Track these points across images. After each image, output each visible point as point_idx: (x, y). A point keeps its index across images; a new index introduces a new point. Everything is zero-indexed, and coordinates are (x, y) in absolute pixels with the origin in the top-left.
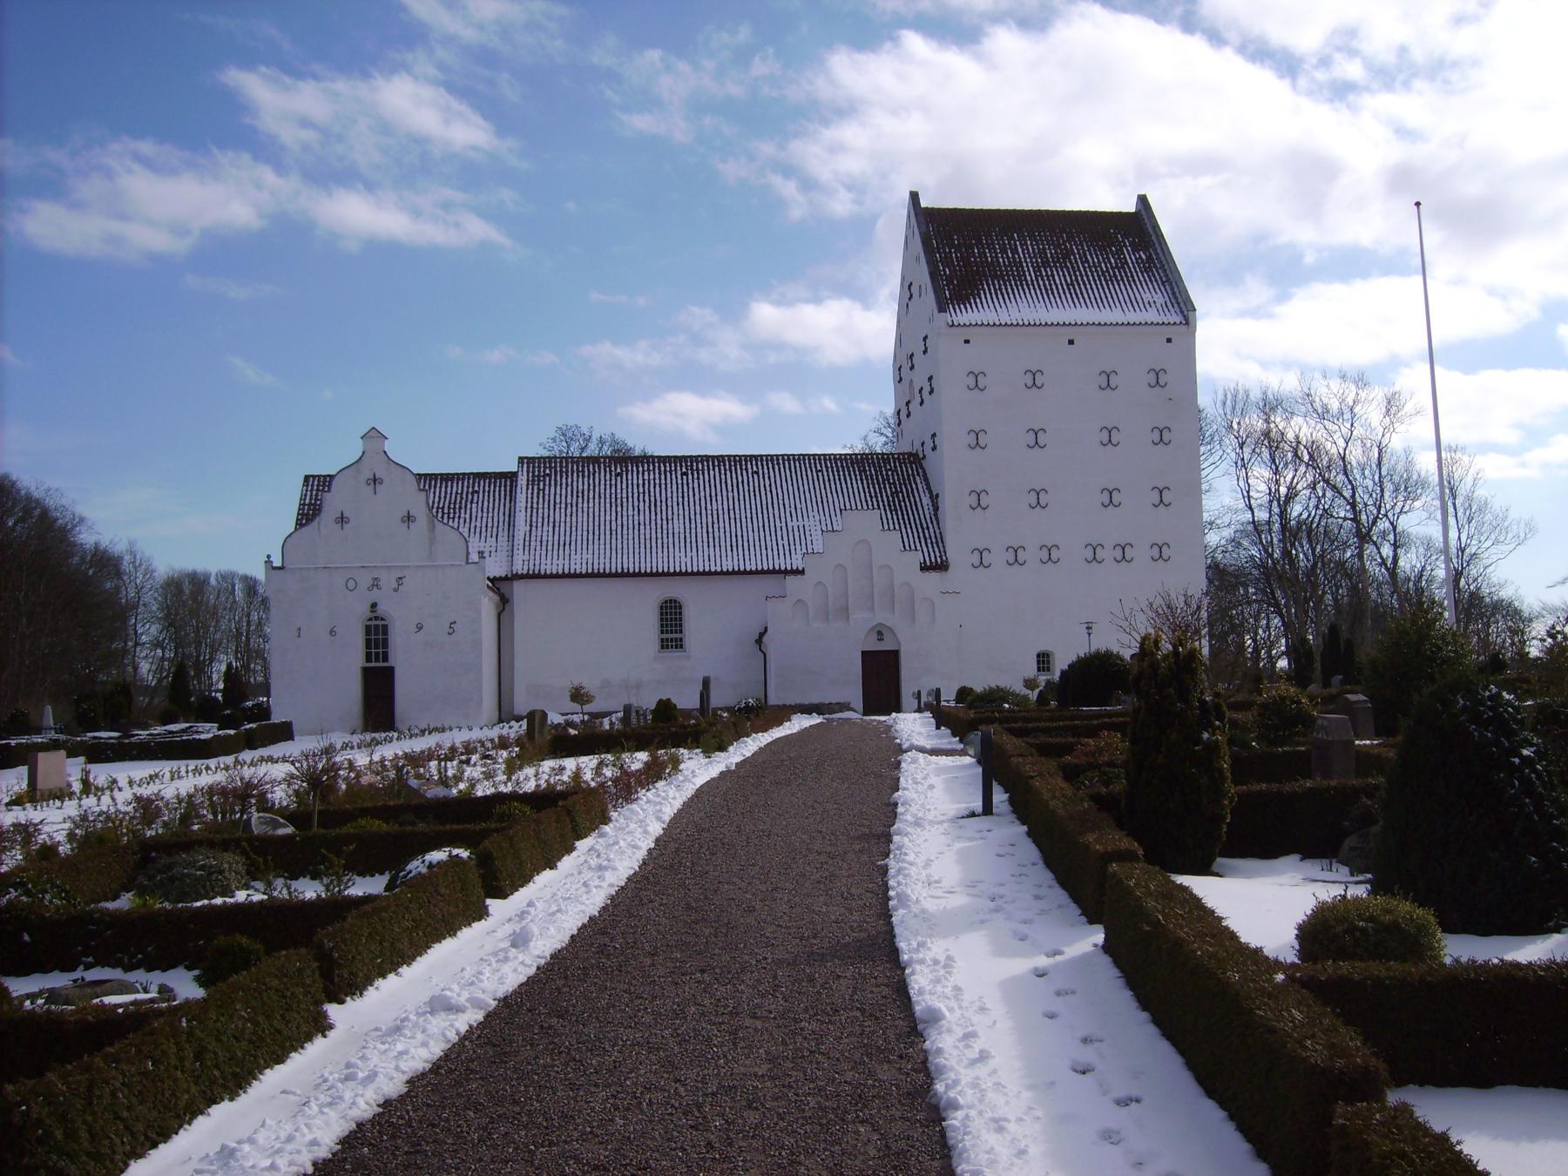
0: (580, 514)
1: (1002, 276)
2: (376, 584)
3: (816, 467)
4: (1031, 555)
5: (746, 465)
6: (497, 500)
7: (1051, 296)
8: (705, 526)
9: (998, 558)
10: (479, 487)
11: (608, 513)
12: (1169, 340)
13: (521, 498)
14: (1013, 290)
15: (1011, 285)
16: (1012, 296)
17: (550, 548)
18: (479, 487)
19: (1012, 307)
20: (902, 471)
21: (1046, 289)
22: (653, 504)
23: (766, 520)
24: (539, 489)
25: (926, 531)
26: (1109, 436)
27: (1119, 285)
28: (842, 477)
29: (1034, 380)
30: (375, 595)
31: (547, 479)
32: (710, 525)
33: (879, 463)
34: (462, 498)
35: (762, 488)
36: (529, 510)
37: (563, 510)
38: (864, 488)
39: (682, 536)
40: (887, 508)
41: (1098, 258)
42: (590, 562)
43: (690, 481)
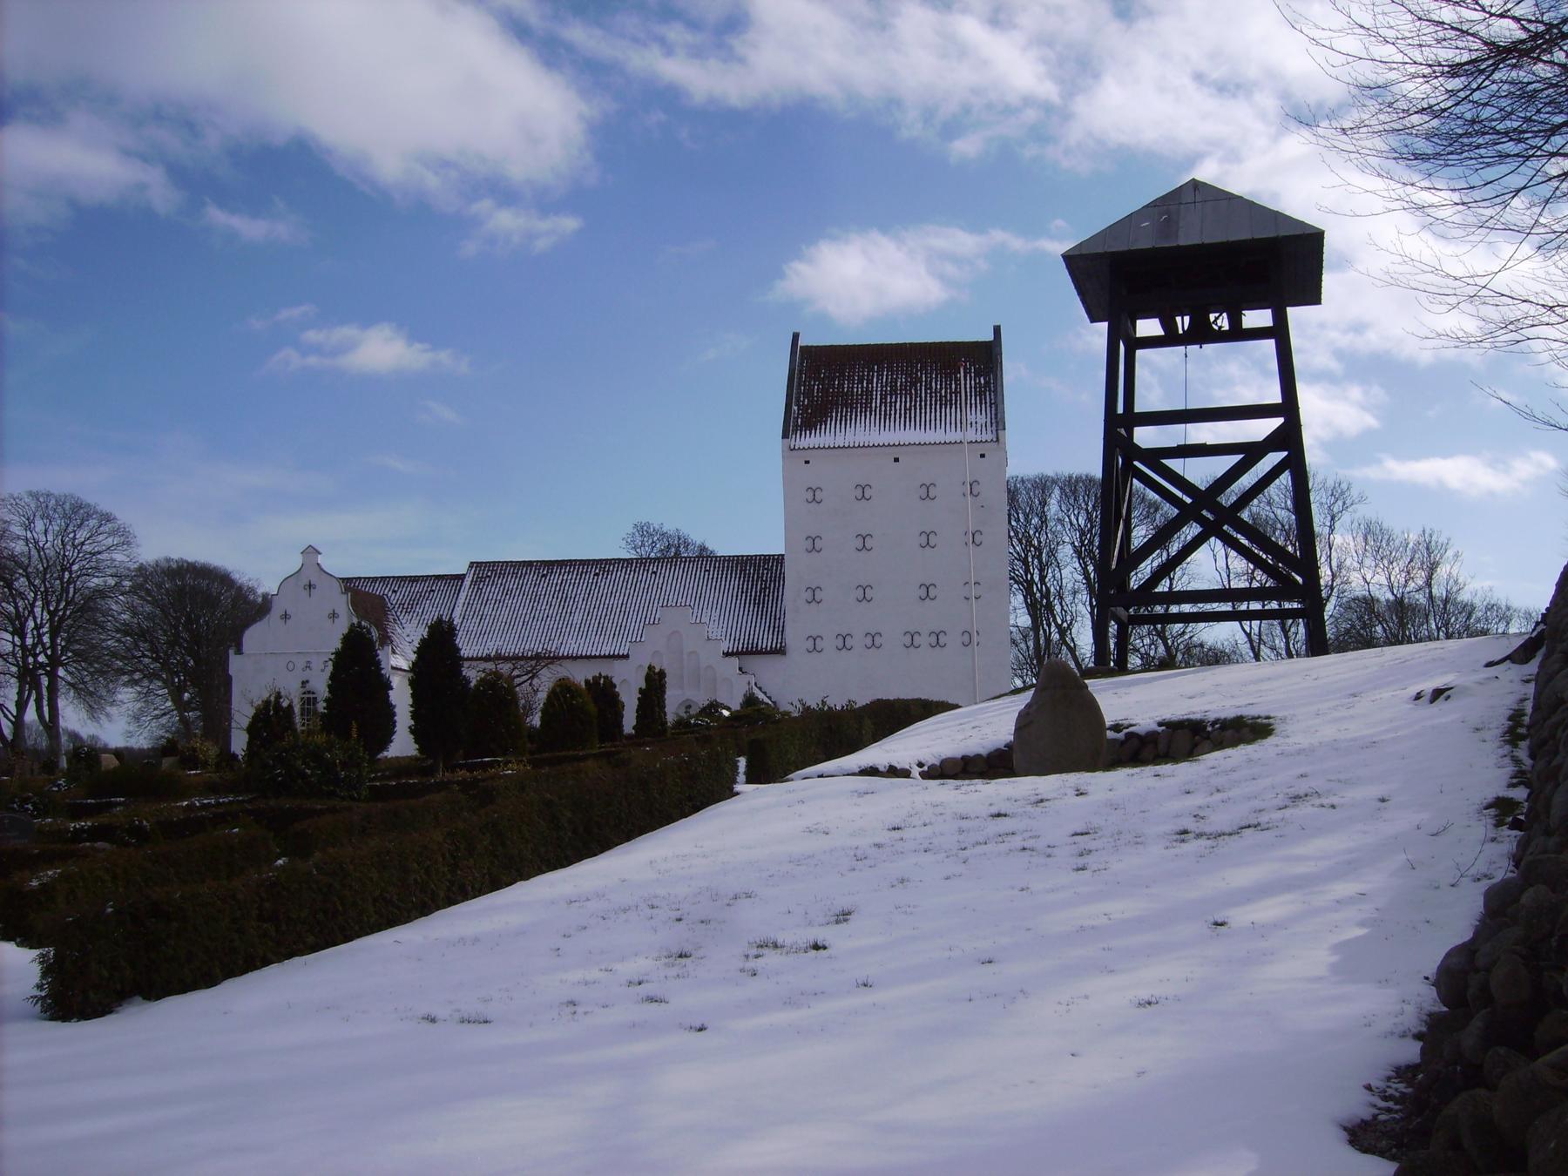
0: (504, 609)
1: (851, 404)
2: (308, 666)
4: (857, 641)
5: (649, 566)
6: (447, 597)
7: (887, 421)
9: (829, 644)
10: (657, 569)
11: (526, 608)
12: (983, 456)
13: (463, 596)
14: (856, 416)
16: (853, 421)
17: (472, 637)
18: (657, 569)
20: (776, 570)
21: (885, 414)
22: (563, 600)
24: (478, 588)
25: (777, 621)
26: (927, 540)
27: (951, 408)
28: (724, 576)
29: (862, 492)
30: (306, 675)
32: (603, 618)
33: (759, 563)
34: (420, 596)
35: (655, 586)
37: (492, 606)
38: (739, 585)
39: (578, 626)
40: (752, 602)
41: (941, 385)
43: (599, 581)
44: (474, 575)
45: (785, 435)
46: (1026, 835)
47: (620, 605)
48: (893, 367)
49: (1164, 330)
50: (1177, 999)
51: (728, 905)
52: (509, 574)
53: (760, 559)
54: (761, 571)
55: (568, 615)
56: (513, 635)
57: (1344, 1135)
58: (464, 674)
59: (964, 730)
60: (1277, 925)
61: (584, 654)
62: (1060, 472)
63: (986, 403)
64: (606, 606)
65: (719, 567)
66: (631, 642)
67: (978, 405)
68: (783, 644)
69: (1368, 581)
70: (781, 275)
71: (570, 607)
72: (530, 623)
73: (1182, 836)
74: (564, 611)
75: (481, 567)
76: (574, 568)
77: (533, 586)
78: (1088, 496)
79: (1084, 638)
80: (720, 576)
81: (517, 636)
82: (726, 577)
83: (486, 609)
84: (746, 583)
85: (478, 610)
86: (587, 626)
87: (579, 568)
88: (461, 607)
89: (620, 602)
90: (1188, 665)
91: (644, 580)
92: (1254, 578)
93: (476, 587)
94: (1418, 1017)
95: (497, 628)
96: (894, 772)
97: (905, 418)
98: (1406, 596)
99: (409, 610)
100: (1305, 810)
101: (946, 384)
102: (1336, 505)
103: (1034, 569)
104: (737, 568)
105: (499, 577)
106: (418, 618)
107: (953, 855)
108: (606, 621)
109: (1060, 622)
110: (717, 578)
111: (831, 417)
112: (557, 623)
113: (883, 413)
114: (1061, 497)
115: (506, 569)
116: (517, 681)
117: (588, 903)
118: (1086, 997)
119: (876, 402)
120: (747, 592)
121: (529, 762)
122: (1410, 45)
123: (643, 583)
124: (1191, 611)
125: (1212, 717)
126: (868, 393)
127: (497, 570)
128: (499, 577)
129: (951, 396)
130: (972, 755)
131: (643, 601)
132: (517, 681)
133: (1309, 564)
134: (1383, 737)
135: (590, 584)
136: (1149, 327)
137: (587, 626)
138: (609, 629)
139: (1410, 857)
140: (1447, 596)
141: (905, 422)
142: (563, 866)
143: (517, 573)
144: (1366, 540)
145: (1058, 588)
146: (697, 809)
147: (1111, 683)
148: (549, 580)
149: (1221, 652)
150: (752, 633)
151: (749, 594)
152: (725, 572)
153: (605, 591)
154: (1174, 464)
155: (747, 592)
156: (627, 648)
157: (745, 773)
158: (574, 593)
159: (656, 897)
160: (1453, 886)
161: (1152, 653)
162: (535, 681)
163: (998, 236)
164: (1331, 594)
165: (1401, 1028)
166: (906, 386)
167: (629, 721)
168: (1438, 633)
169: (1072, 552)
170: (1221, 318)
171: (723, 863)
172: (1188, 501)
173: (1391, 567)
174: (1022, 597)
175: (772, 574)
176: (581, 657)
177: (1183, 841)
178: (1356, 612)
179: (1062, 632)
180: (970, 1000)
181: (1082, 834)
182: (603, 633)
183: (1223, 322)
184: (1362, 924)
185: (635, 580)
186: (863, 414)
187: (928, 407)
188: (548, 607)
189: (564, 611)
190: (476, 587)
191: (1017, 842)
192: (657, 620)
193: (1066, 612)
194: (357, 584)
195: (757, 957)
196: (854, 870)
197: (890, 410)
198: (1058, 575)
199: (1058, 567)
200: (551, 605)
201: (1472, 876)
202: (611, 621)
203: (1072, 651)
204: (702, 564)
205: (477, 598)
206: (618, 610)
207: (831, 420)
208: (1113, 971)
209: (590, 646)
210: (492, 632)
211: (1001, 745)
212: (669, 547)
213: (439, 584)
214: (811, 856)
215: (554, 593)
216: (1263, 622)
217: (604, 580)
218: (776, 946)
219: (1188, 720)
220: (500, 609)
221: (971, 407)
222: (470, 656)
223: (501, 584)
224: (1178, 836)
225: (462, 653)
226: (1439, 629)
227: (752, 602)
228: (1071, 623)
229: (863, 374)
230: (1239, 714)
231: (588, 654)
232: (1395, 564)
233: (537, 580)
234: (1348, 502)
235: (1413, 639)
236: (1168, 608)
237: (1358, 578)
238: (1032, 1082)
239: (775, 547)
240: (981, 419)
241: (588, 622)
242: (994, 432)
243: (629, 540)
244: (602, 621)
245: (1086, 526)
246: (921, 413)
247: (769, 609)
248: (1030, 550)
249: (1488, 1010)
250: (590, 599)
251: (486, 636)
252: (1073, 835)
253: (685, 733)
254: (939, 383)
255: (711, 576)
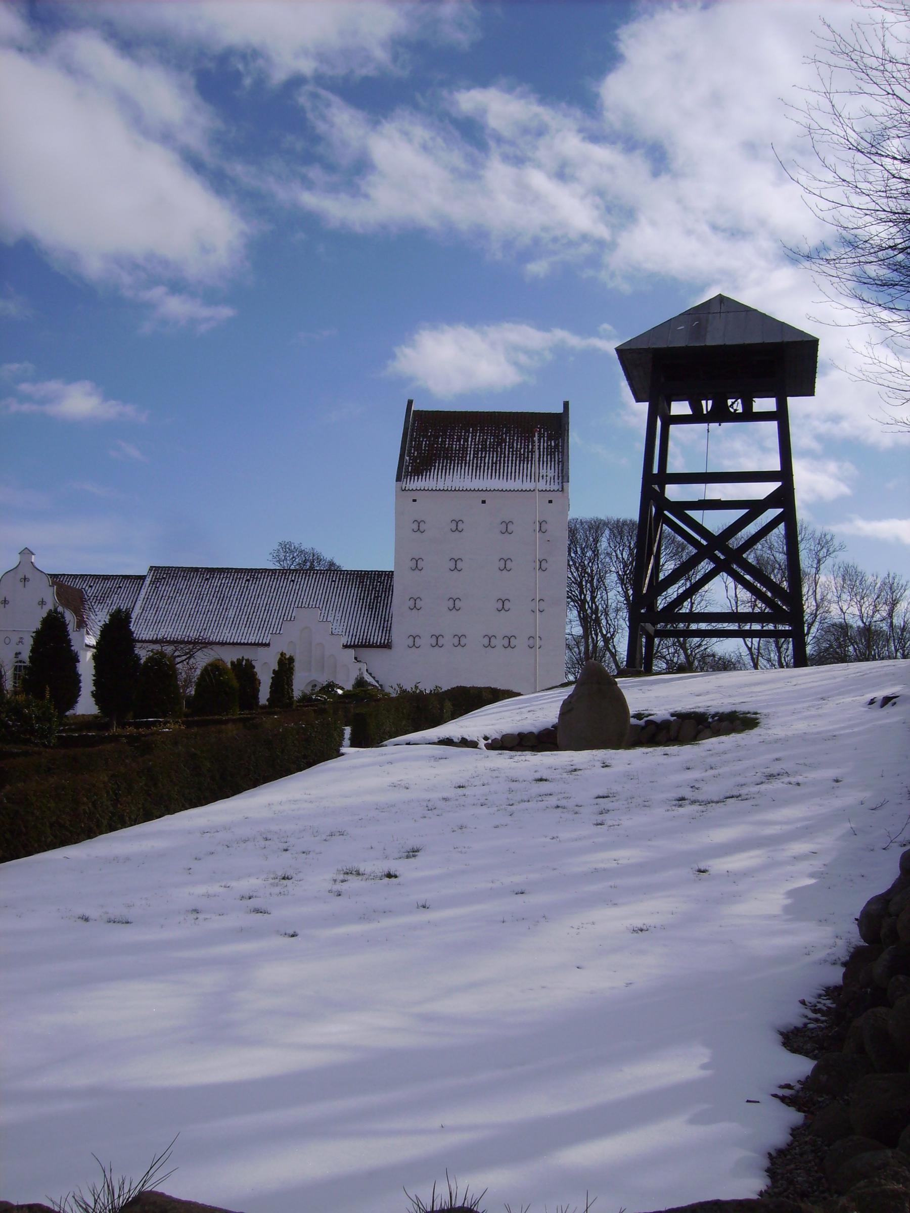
0: (175, 603)
1: (451, 457)
3: (332, 578)
5: (289, 576)
6: (131, 593)
7: (478, 471)
8: (248, 614)
9: (425, 641)
10: (295, 578)
11: (192, 604)
12: (550, 502)
13: (143, 592)
14: (454, 466)
15: (454, 464)
16: (452, 470)
17: (150, 624)
18: (295, 578)
19: (457, 476)
20: (387, 583)
21: (477, 466)
22: (221, 599)
23: (287, 612)
24: (156, 587)
25: (386, 623)
26: (505, 565)
27: (527, 464)
28: (347, 586)
29: (457, 526)
30: (19, 648)
31: (163, 580)
32: (251, 614)
33: (374, 577)
34: (111, 591)
36: (145, 600)
37: (165, 601)
38: (357, 593)
39: (232, 619)
40: (367, 607)
41: (521, 445)
42: (170, 633)
43: (250, 585)
44: (153, 576)
45: (398, 479)
46: (560, 796)
47: (264, 605)
48: (484, 430)
49: (692, 411)
50: (663, 928)
51: (325, 840)
52: (180, 576)
53: (375, 574)
54: (375, 584)
55: (224, 610)
56: (181, 625)
57: (780, 1038)
58: (136, 652)
59: (521, 713)
60: (746, 874)
61: (231, 642)
62: (610, 517)
63: (555, 461)
64: (254, 605)
65: (343, 579)
66: (272, 634)
67: (549, 462)
68: (390, 641)
69: (844, 611)
70: (393, 357)
71: (226, 605)
72: (194, 616)
73: (680, 802)
74: (222, 607)
75: (158, 570)
76: (231, 575)
77: (198, 587)
78: (631, 536)
79: (622, 645)
80: (343, 586)
81: (184, 624)
82: (348, 588)
83: (161, 603)
84: (363, 592)
85: (154, 603)
86: (239, 619)
87: (234, 575)
88: (141, 601)
89: (265, 602)
90: (702, 670)
91: (284, 586)
92: (756, 605)
93: (154, 586)
94: (847, 950)
95: (169, 618)
96: (465, 743)
97: (492, 470)
98: (873, 624)
99: (101, 601)
100: (776, 785)
101: (525, 445)
102: (822, 552)
103: (587, 591)
104: (357, 580)
105: (172, 579)
106: (108, 607)
107: (502, 809)
108: (254, 617)
109: (605, 632)
110: (341, 587)
111: (435, 466)
112: (215, 616)
113: (475, 465)
114: (610, 536)
115: (177, 574)
116: (178, 660)
117: (216, 833)
118: (593, 923)
119: (470, 457)
120: (363, 599)
121: (183, 723)
122: (880, 196)
123: (283, 588)
124: (707, 628)
125: (712, 711)
126: (464, 449)
127: (170, 573)
128: (172, 579)
129: (528, 455)
130: (526, 732)
131: (283, 603)
132: (178, 660)
133: (795, 597)
134: (842, 732)
135: (242, 588)
136: (680, 408)
137: (239, 619)
138: (256, 622)
139: (853, 826)
140: (904, 626)
141: (492, 472)
142: (202, 805)
143: (186, 577)
144: (844, 580)
145: (605, 606)
146: (310, 765)
147: (638, 682)
148: (211, 583)
149: (729, 661)
150: (366, 631)
151: (365, 601)
152: (347, 583)
153: (254, 594)
154: (695, 515)
155: (363, 599)
156: (268, 638)
157: (350, 739)
158: (230, 593)
159: (270, 832)
160: (884, 849)
161: (675, 660)
162: (192, 661)
163: (560, 334)
164: (814, 620)
165: (834, 958)
166: (494, 445)
167: (264, 695)
168: (896, 653)
169: (616, 579)
170: (736, 403)
171: (325, 807)
172: (705, 543)
173: (862, 601)
174: (576, 612)
175: (383, 585)
176: (229, 644)
177: (680, 806)
178: (834, 635)
179: (607, 640)
180: (503, 922)
181: (604, 797)
182: (251, 626)
183: (738, 407)
184: (812, 875)
185: (277, 586)
186: (460, 465)
187: (510, 462)
188: (209, 604)
189: (222, 607)
190: (154, 586)
191: (553, 801)
192: (293, 618)
193: (610, 625)
194: (62, 579)
195: (343, 881)
196: (425, 817)
197: (481, 463)
198: (605, 597)
199: (606, 590)
200: (211, 603)
201: (900, 842)
202: (257, 617)
203: (613, 655)
204: (330, 576)
205: (154, 594)
206: (263, 608)
207: (435, 469)
208: (616, 904)
209: (240, 636)
210: (164, 622)
211: (549, 726)
212: (305, 562)
213: (126, 582)
214: (393, 806)
215: (214, 593)
216: (762, 639)
217: (253, 585)
218: (358, 874)
219: (695, 713)
220: (171, 604)
221: (543, 463)
222: (147, 639)
223: (173, 585)
224: (677, 802)
225: (135, 635)
226: (897, 651)
227: (367, 607)
228: (614, 634)
229: (461, 435)
230: (734, 710)
231: (239, 642)
232: (865, 599)
233: (201, 582)
234: (831, 550)
235: (877, 657)
236: (689, 625)
237: (836, 609)
238: (543, 987)
239: (385, 563)
240: (551, 473)
241: (240, 617)
242: (560, 483)
243: (275, 555)
244: (250, 617)
245: (628, 559)
246: (504, 466)
247: (380, 613)
248: (584, 577)
249: (894, 946)
250: (242, 599)
251: (160, 624)
252: (597, 798)
253: (306, 706)
254: (519, 444)
255: (336, 586)
